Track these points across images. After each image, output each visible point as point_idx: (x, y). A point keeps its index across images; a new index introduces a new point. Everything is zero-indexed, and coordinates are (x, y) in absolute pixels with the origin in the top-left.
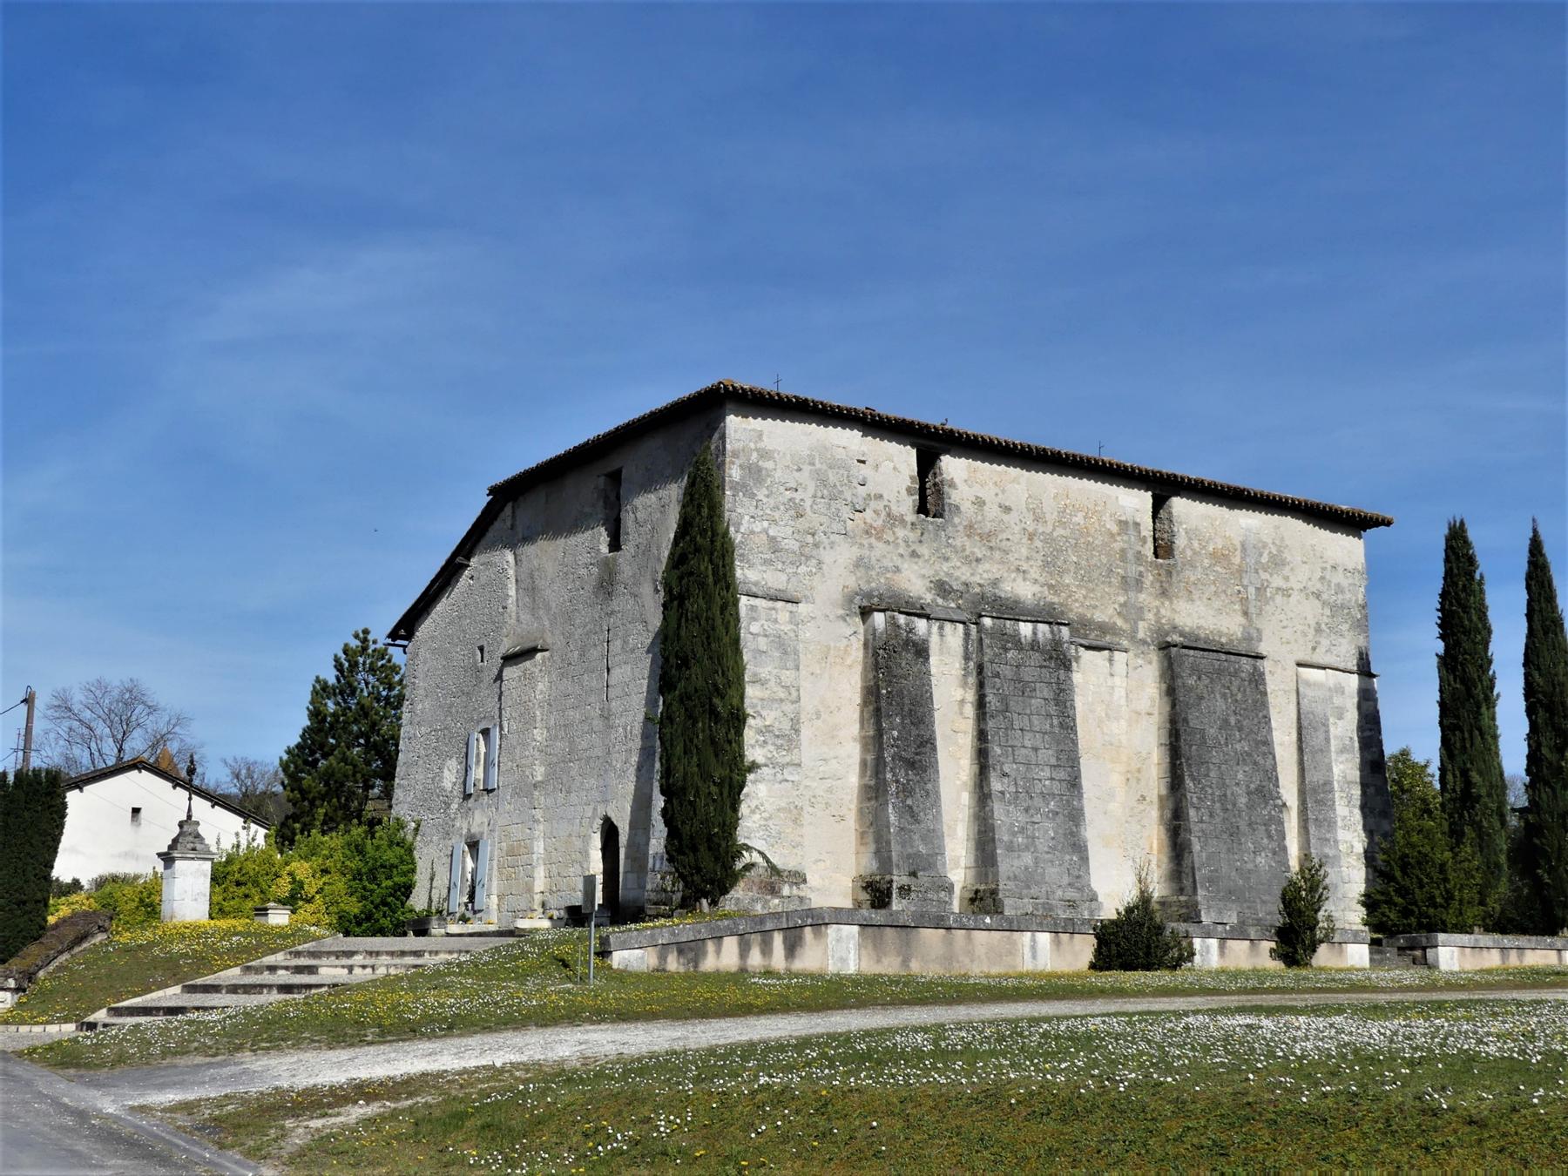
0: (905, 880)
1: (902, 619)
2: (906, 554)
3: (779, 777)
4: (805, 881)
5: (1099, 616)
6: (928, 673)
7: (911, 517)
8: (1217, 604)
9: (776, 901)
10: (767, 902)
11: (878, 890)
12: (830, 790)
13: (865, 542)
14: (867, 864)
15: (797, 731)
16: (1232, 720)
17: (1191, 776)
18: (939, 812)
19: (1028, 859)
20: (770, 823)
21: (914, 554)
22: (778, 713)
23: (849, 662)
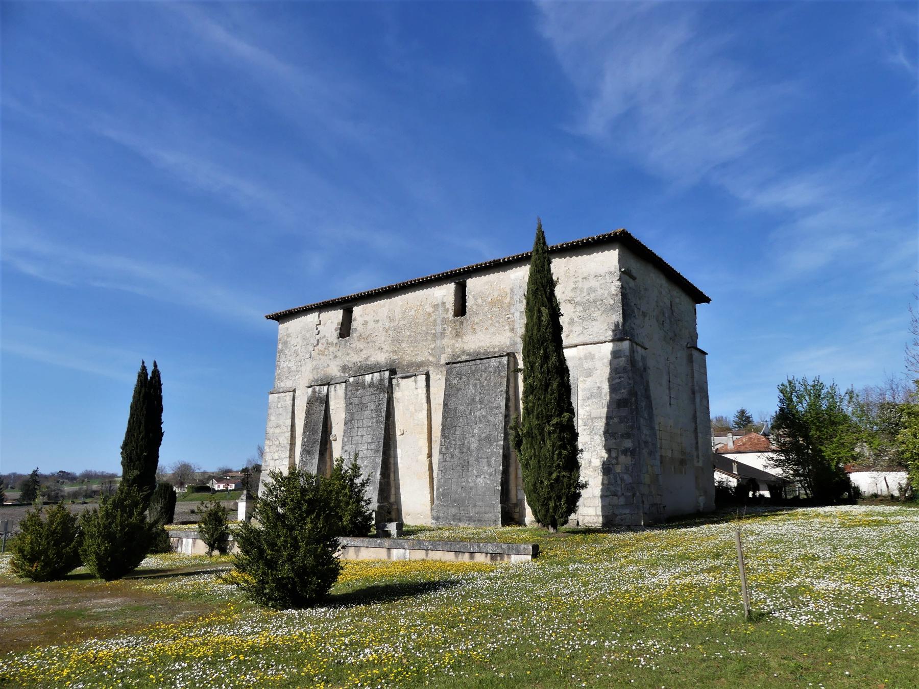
1: (317, 388)
5: (420, 359)
7: (336, 341)
8: (492, 330)
16: (477, 399)
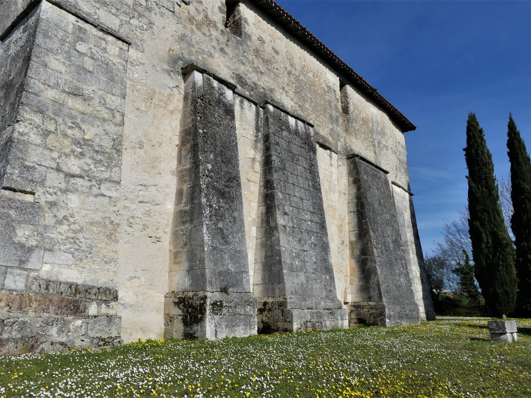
0: (217, 296)
1: (215, 84)
2: (217, 48)
3: (95, 190)
4: (116, 298)
6: (234, 128)
7: (221, 26)
9: (79, 322)
10: (66, 323)
11: (191, 306)
12: (148, 213)
13: (188, 26)
14: (181, 281)
15: (119, 151)
17: (372, 229)
18: (243, 237)
19: (302, 278)
20: (80, 236)
21: (222, 50)
22: (100, 131)
23: (170, 108)
